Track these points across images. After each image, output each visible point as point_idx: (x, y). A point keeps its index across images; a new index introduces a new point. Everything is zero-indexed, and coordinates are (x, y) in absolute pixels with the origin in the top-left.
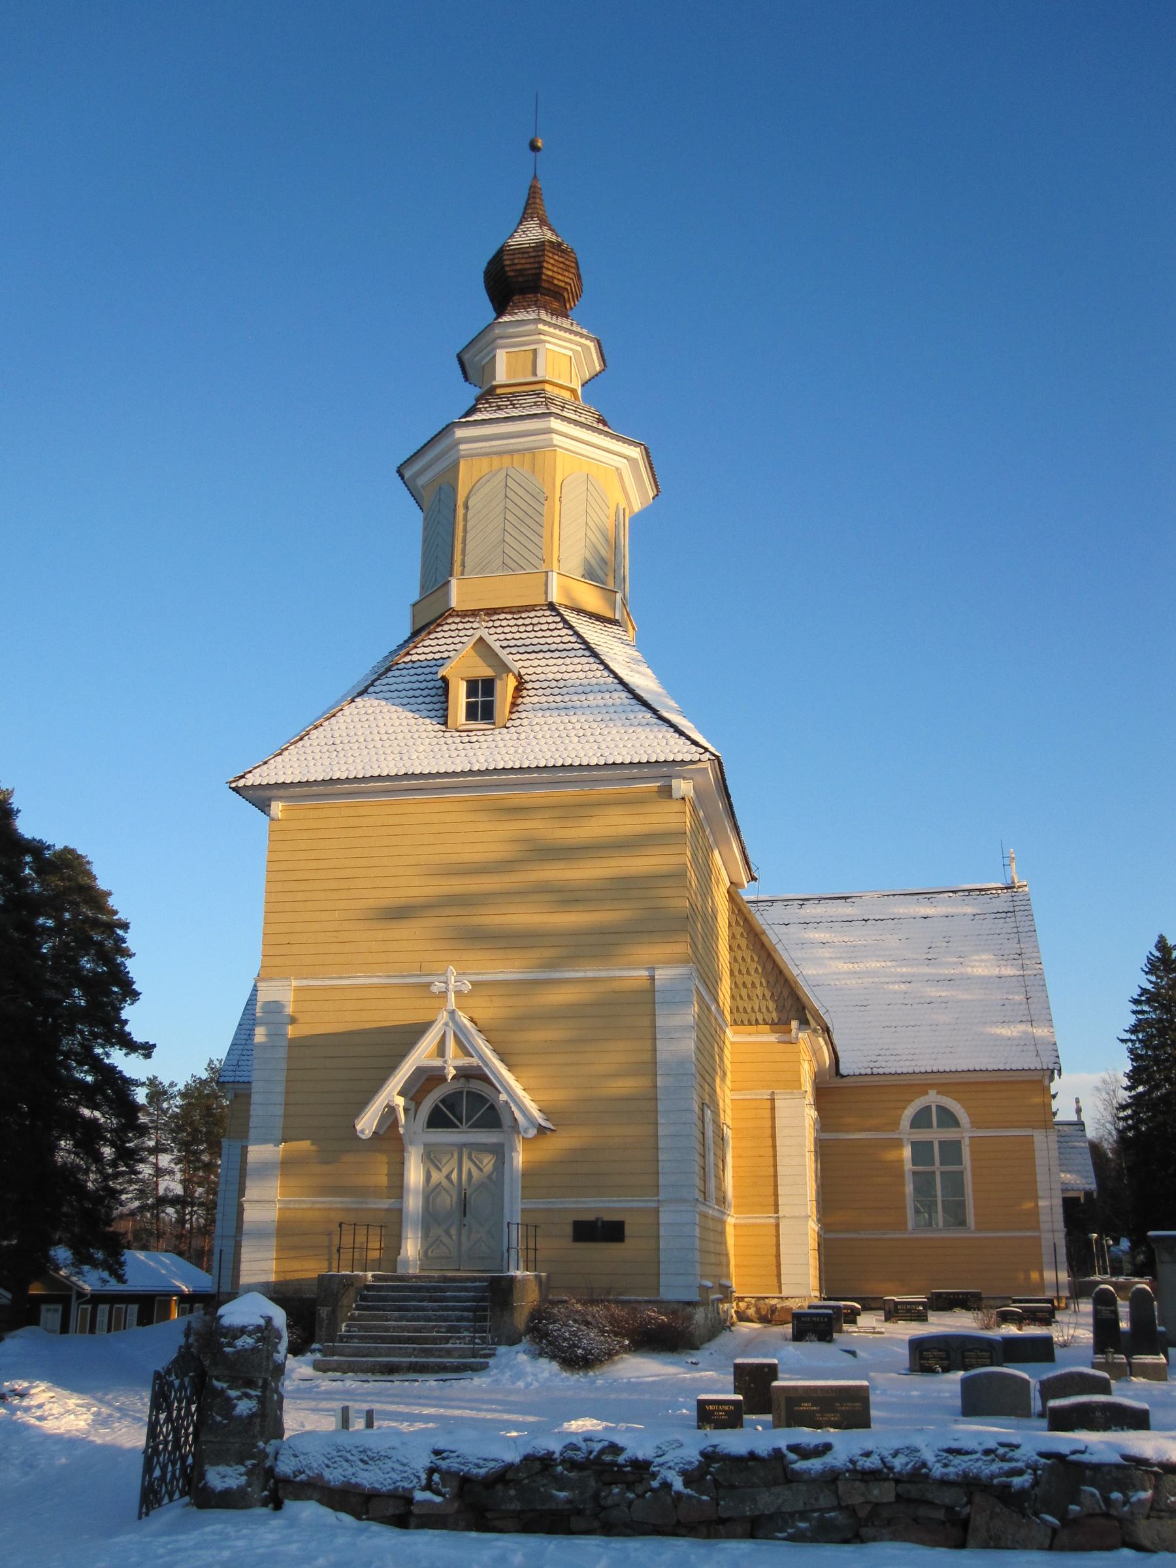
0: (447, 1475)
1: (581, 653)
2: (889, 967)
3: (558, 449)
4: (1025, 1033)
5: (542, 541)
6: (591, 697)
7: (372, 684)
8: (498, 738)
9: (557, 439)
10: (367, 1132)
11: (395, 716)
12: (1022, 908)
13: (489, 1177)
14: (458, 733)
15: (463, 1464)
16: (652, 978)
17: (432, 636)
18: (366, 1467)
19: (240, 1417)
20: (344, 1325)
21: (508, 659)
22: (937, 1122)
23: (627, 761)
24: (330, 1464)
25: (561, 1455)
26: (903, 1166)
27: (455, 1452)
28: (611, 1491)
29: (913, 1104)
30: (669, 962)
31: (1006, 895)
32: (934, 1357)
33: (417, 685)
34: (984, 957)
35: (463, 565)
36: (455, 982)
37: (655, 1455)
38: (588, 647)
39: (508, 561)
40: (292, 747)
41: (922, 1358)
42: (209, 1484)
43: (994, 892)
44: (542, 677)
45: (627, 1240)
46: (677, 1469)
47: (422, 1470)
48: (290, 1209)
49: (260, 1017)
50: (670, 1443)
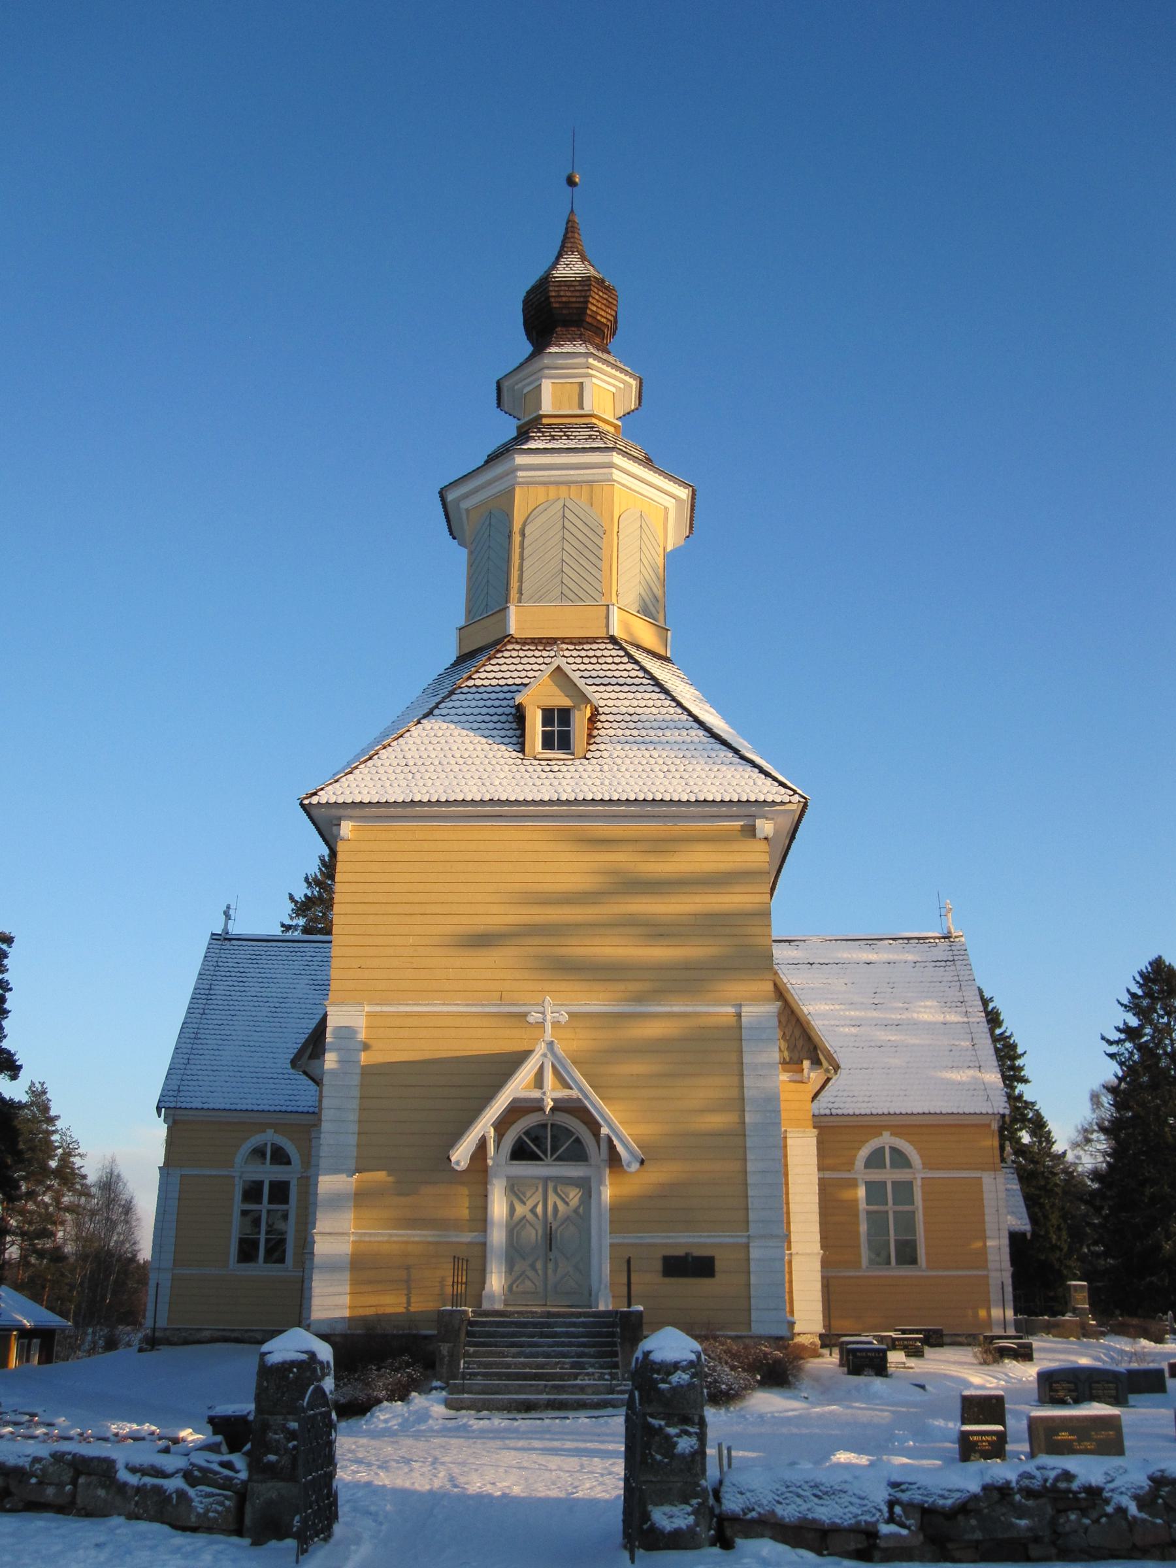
0: (909, 1507)
1: (650, 688)
2: (837, 1010)
3: (615, 484)
4: (974, 1078)
5: (601, 575)
6: (668, 733)
7: (437, 707)
8: (581, 768)
9: (617, 475)
10: (462, 1163)
11: (467, 740)
12: (961, 958)
13: (576, 1211)
14: (538, 762)
15: (927, 1496)
16: (739, 1015)
17: (493, 662)
18: (821, 1502)
19: (682, 1456)
20: (462, 1362)
21: (589, 691)
22: (890, 1161)
23: (718, 799)
24: (781, 1500)
25: (1017, 1483)
26: (857, 1205)
27: (915, 1483)
28: (1068, 1517)
29: (867, 1145)
30: (754, 1000)
31: (944, 944)
32: (1063, 1389)
33: (484, 711)
34: (928, 1003)
35: (520, 592)
36: (552, 1013)
37: (1105, 1481)
38: (657, 683)
39: (566, 591)
40: (363, 766)
41: (1051, 1390)
42: (657, 1525)
43: (932, 941)
44: (615, 710)
45: (718, 1275)
46: (1129, 1494)
47: (883, 1503)
48: (364, 1242)
49: (331, 1042)
50: (1117, 1469)
